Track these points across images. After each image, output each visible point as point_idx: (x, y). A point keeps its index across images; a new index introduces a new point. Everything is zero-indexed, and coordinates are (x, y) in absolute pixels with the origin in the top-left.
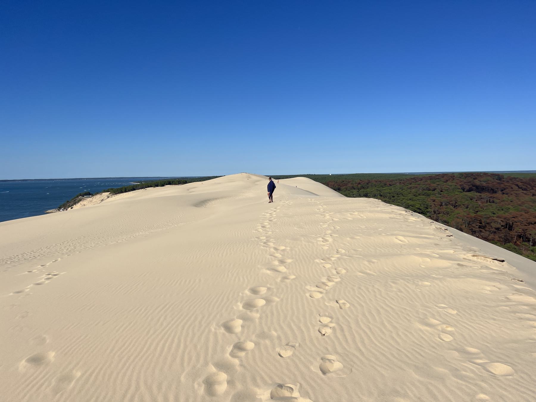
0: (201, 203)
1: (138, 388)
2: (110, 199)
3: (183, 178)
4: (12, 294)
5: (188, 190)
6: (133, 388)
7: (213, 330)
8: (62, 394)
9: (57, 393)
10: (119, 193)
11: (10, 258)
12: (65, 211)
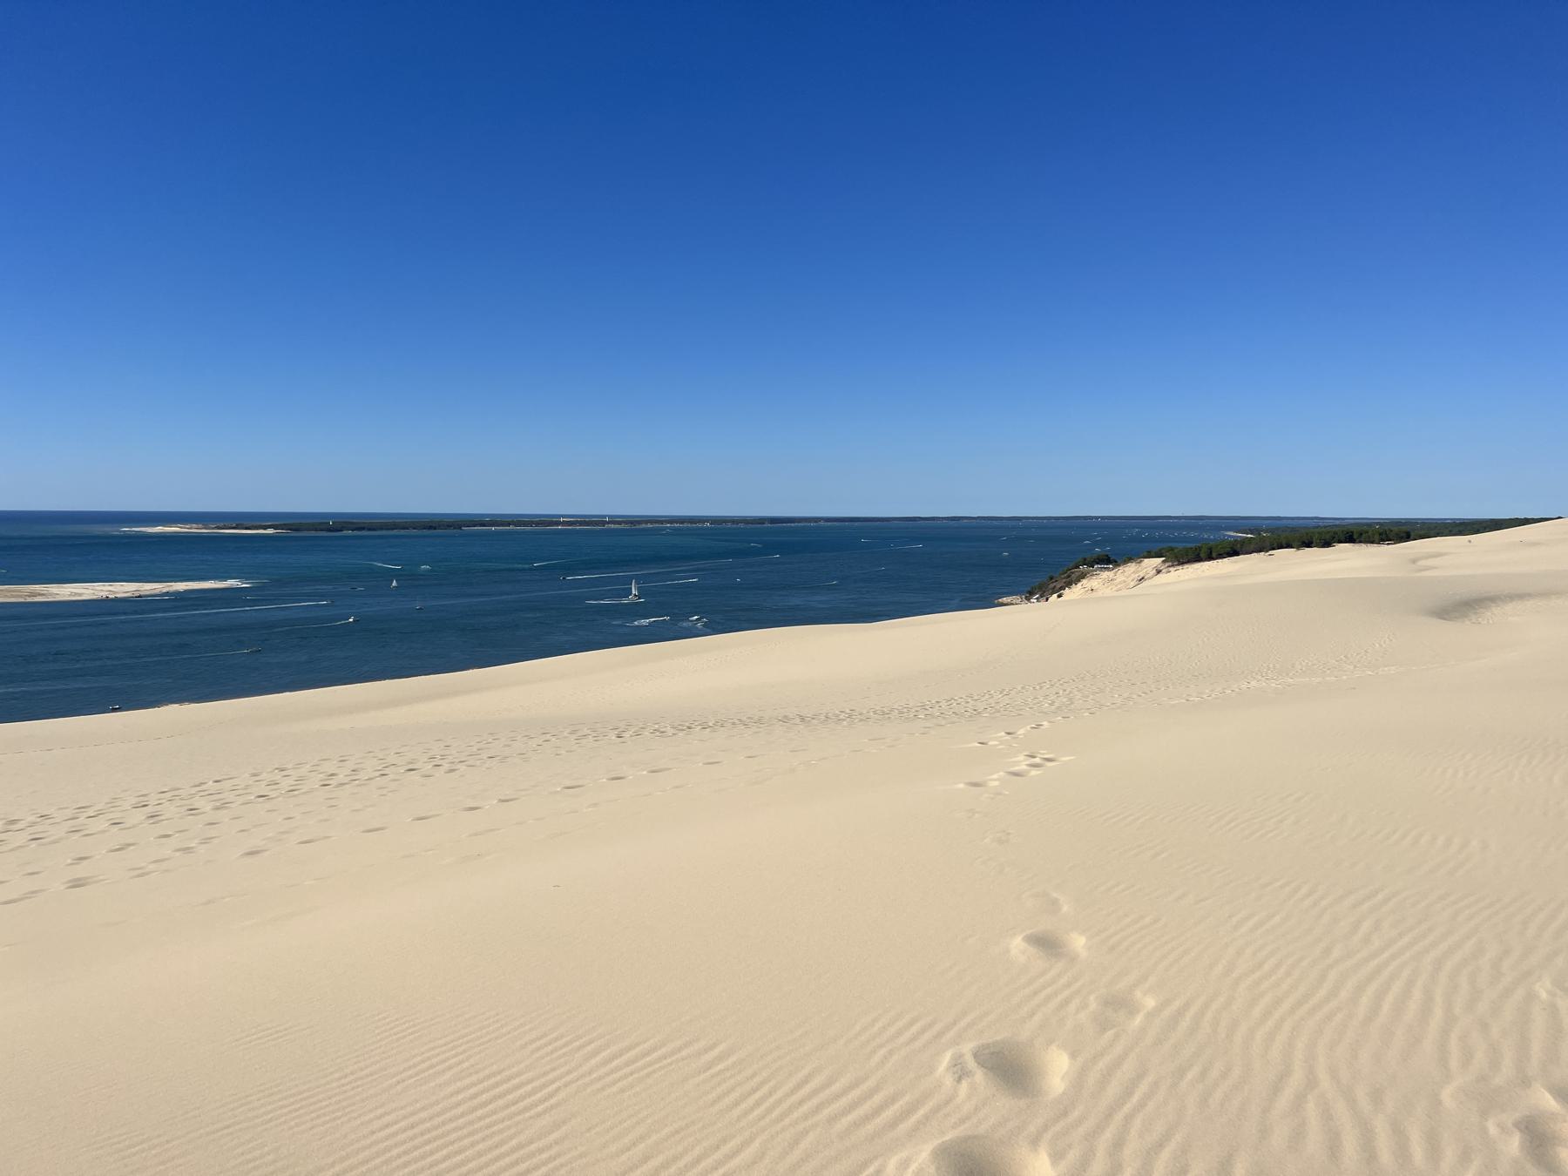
0: (1462, 606)
1: (1311, 1082)
2: (1163, 578)
3: (1398, 522)
4: (961, 786)
5: (1414, 561)
6: (1297, 1078)
7: (1544, 995)
8: (1117, 1036)
9: (1104, 1030)
10: (1189, 562)
11: (923, 707)
12: (1043, 604)
